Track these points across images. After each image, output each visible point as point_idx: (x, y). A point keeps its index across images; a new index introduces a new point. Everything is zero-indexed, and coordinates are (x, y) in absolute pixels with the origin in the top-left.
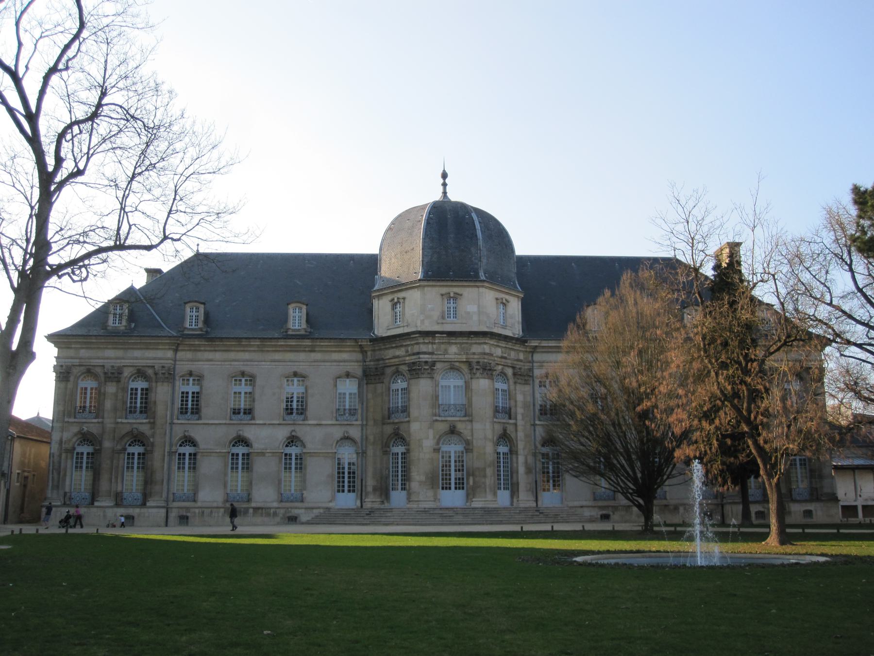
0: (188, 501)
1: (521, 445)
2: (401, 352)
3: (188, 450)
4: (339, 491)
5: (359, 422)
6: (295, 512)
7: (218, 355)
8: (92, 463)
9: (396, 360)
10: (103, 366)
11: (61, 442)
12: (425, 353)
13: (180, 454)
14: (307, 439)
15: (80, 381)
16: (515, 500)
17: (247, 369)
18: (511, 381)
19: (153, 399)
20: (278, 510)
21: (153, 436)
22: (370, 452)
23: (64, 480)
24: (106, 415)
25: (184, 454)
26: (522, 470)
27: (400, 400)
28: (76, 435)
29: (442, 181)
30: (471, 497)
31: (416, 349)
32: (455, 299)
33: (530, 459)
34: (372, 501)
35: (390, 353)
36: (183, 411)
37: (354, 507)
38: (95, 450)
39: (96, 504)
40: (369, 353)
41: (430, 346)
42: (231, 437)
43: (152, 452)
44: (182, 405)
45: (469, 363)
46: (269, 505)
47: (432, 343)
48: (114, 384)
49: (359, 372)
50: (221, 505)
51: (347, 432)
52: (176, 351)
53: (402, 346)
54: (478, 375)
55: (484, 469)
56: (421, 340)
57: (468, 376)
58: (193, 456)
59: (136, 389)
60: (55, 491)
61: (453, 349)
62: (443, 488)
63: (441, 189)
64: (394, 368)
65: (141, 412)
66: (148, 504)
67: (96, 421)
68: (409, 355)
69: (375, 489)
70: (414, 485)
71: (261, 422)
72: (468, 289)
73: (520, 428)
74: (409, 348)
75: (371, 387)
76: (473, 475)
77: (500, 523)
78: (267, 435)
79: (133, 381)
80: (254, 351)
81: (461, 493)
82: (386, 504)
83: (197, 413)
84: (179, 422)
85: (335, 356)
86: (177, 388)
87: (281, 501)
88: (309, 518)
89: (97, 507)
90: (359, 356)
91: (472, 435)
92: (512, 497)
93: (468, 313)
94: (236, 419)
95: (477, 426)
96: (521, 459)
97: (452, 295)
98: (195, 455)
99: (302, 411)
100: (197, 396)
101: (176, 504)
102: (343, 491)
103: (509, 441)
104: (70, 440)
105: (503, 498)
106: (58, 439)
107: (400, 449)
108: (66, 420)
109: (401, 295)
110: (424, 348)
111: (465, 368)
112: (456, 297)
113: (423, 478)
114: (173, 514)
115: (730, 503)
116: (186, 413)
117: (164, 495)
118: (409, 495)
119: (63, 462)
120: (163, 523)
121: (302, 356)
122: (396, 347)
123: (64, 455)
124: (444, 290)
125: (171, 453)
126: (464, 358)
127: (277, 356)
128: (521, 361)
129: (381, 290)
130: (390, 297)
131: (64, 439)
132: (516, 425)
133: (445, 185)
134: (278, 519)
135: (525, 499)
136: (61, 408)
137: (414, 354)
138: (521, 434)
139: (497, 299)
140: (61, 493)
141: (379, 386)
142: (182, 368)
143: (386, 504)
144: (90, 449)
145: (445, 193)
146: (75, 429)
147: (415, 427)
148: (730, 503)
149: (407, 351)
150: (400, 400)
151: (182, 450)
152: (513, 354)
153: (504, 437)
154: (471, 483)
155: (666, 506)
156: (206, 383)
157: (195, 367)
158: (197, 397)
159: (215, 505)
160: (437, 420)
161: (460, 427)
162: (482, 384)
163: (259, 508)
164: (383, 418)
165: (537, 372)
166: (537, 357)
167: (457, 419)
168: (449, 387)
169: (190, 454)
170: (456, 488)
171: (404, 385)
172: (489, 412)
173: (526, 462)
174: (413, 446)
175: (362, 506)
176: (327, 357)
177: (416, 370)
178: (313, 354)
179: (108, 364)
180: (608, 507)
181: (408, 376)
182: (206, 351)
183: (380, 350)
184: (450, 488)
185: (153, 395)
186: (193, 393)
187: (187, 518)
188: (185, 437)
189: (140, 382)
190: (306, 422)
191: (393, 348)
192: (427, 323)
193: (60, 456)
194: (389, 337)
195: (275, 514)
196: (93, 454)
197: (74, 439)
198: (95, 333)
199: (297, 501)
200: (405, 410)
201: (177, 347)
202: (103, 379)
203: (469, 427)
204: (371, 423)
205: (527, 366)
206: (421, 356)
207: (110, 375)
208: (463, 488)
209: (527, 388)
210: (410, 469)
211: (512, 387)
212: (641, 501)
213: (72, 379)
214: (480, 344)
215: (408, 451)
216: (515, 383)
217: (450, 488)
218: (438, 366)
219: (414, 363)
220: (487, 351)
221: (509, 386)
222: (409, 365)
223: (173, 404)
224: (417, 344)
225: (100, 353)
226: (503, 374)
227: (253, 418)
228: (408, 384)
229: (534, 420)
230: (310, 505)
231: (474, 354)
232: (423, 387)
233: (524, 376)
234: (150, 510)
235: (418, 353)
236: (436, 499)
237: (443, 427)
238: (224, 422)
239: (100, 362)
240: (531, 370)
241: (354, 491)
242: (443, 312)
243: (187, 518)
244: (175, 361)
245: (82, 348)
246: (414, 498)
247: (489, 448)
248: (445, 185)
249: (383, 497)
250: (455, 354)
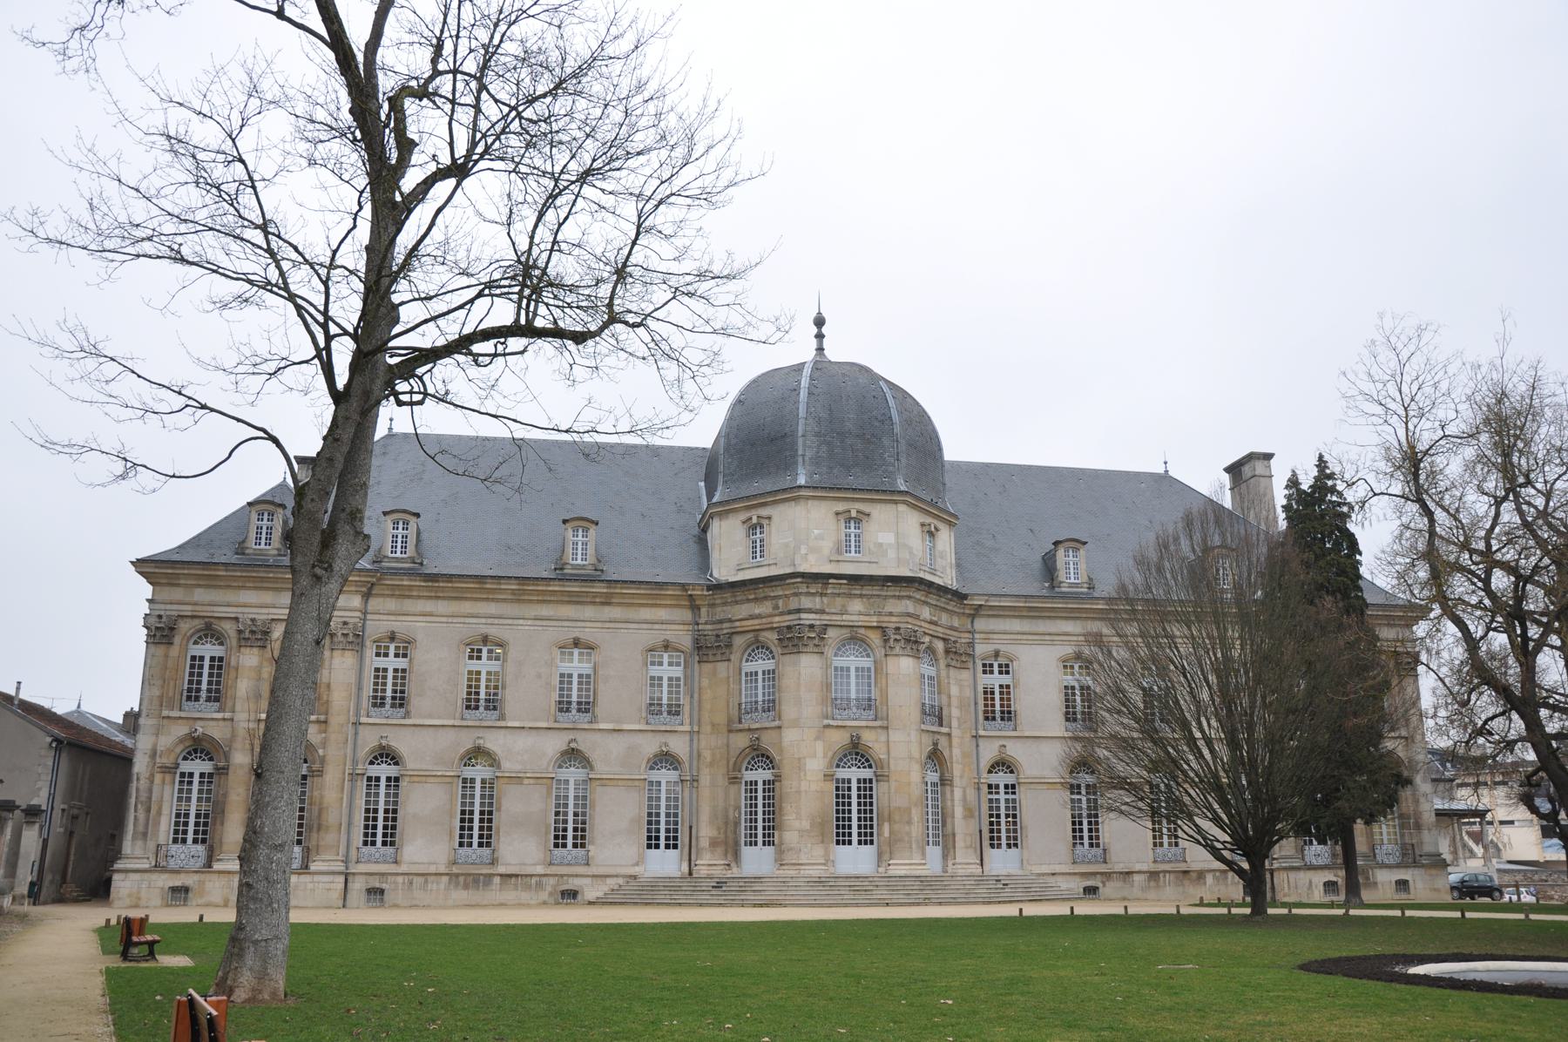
0: (385, 862)
1: (957, 770)
2: (764, 608)
3: (384, 770)
4: (649, 846)
5: (687, 728)
6: (573, 884)
7: (442, 607)
8: (209, 791)
9: (756, 622)
10: (236, 619)
11: (154, 754)
12: (810, 611)
13: (369, 779)
14: (595, 757)
15: (191, 645)
16: (950, 863)
17: (493, 631)
18: (942, 663)
19: (325, 680)
20: (544, 880)
21: (324, 744)
22: (705, 780)
23: (157, 823)
24: (238, 707)
25: (378, 779)
26: (959, 811)
27: (760, 691)
28: (181, 741)
29: (815, 330)
30: (886, 857)
31: (794, 604)
32: (858, 521)
33: (971, 794)
34: (709, 864)
35: (743, 610)
36: (378, 702)
37: (678, 874)
38: (217, 768)
39: (217, 866)
40: (704, 610)
41: (818, 599)
42: (462, 750)
43: (320, 773)
44: (375, 691)
45: (882, 629)
46: (529, 870)
47: (822, 595)
48: (255, 650)
49: (685, 639)
50: (442, 870)
51: (666, 745)
52: (367, 596)
53: (766, 598)
54: (897, 650)
55: (909, 810)
56: (803, 589)
57: (879, 653)
58: (393, 781)
59: (202, 658)
60: (140, 843)
61: (856, 606)
62: (838, 843)
63: (814, 343)
64: (750, 635)
65: (208, 699)
66: (313, 867)
67: (220, 715)
68: (782, 614)
69: (714, 844)
70: (790, 837)
71: (517, 724)
72: (879, 506)
73: (955, 741)
74: (780, 603)
75: (707, 667)
76: (889, 820)
77: (954, 902)
78: (525, 747)
79: (196, 643)
80: (504, 600)
81: (868, 851)
82: (735, 870)
83: (401, 705)
84: (371, 721)
85: (646, 613)
86: (367, 661)
87: (551, 864)
88: (600, 894)
89: (220, 872)
90: (687, 615)
91: (889, 753)
92: (945, 857)
93: (881, 545)
94: (565, 720)
95: (895, 736)
96: (958, 793)
97: (854, 514)
98: (397, 779)
99: (585, 707)
100: (400, 674)
101: (362, 868)
102: (657, 846)
103: (941, 765)
104: (170, 751)
105: (931, 862)
106: (149, 746)
107: (761, 775)
108: (165, 713)
109: (764, 512)
110: (806, 602)
111: (875, 638)
112: (859, 520)
113: (806, 825)
114: (358, 885)
115: (1285, 869)
116: (382, 705)
117: (342, 850)
118: (780, 853)
119: (156, 789)
120: (340, 903)
121: (588, 612)
122: (756, 600)
123: (158, 778)
124: (841, 507)
125: (354, 776)
126: (874, 621)
127: (545, 611)
128: (955, 629)
129: (728, 502)
130: (743, 516)
131: (159, 749)
132: (949, 735)
133: (820, 336)
134: (544, 896)
135: (965, 860)
136: (156, 692)
137: (790, 612)
138: (956, 752)
139: (923, 525)
140: (151, 845)
141: (722, 666)
142: (377, 626)
143: (735, 870)
144: (207, 767)
145: (820, 349)
146: (182, 730)
147: (790, 736)
148: (1285, 869)
149: (776, 607)
150: (760, 691)
151: (374, 771)
152: (944, 619)
153: (935, 757)
154: (886, 834)
155: (1185, 872)
156: (418, 654)
157: (400, 626)
158: (403, 678)
159: (432, 869)
160: (828, 726)
161: (868, 738)
162: (904, 666)
163: (510, 876)
164: (730, 721)
165: (981, 649)
166: (980, 624)
167: (864, 723)
168: (848, 669)
169: (389, 779)
170: (860, 843)
171: (769, 664)
172: (916, 714)
173: (964, 799)
174: (786, 770)
175: (690, 874)
176: (632, 614)
177: (793, 640)
178: (607, 609)
179: (247, 614)
180: (1094, 874)
181: (777, 650)
182: (419, 597)
183: (725, 604)
184: (850, 843)
185: (325, 672)
186: (580, 676)
187: (382, 891)
188: (382, 747)
189: (208, 646)
190: (595, 726)
191: (748, 601)
192: (812, 558)
193: (152, 776)
194: (743, 583)
195: (539, 886)
196: (211, 775)
197: (178, 750)
198: (223, 560)
199: (577, 864)
200: (771, 706)
201: (370, 589)
202: (234, 642)
203: (883, 738)
204: (707, 728)
205: (965, 638)
206: (803, 616)
207: (247, 635)
208: (872, 842)
209: (965, 675)
210: (781, 809)
211: (943, 673)
212: (1246, 866)
213: (177, 640)
214: (900, 598)
215: (778, 778)
216: (948, 666)
217: (850, 843)
218: (831, 633)
219: (789, 627)
220: (911, 610)
221: (938, 671)
222: (779, 630)
223: (360, 689)
224: (796, 594)
225: (230, 596)
226: (931, 650)
227: (502, 717)
228: (777, 664)
229: (357, 714)
230: (601, 871)
231: (891, 614)
232: (805, 669)
233: (958, 655)
234: (317, 878)
235: (799, 611)
236: (828, 861)
237: (840, 739)
238: (451, 722)
239: (231, 611)
240: (971, 644)
241: (675, 847)
242: (839, 542)
243: (382, 891)
244: (365, 613)
245: (199, 586)
246: (789, 858)
247: (915, 776)
248: (820, 336)
249: (730, 856)
250: (860, 614)
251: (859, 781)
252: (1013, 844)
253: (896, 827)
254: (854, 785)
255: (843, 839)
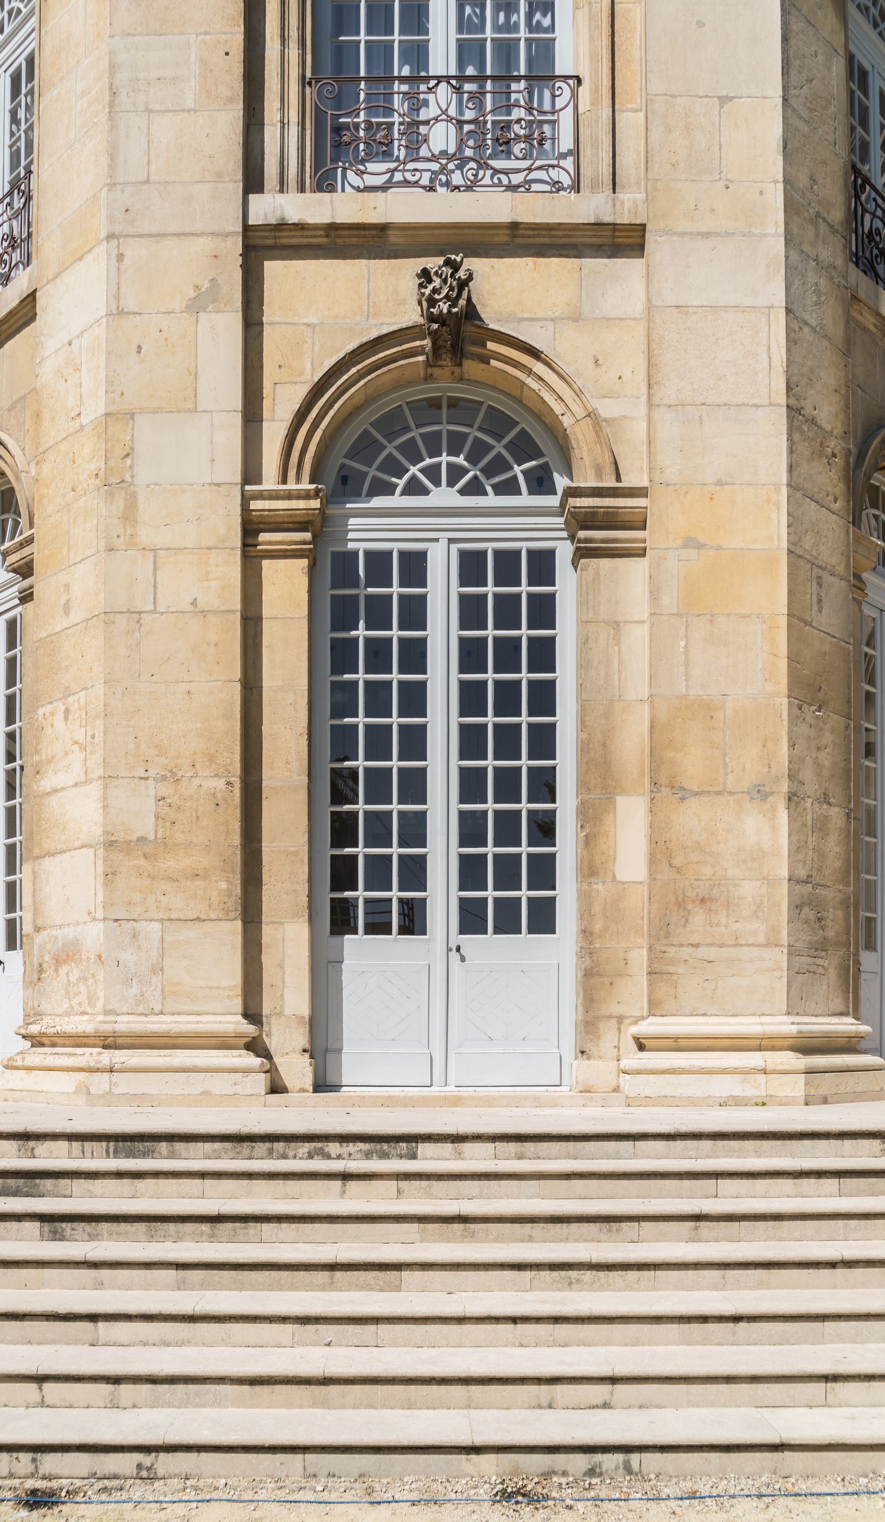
30: (632, 993)
170: (471, 919)
184: (413, 920)
208: (543, 919)
217: (413, 920)
251: (471, 566)
252: (512, 891)
253: (690, 819)
254: (442, 590)
255: (360, 891)
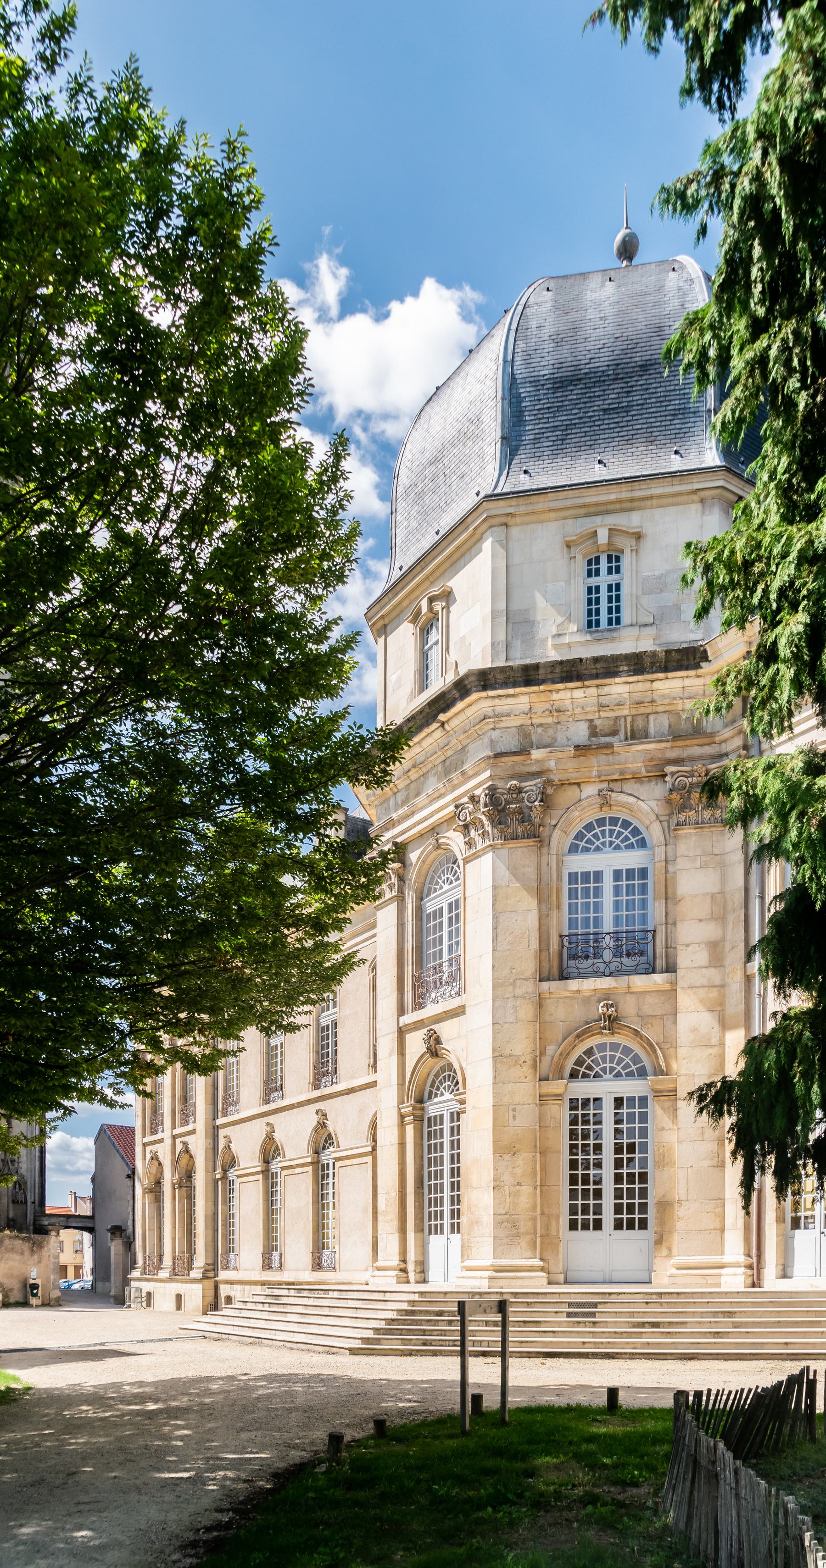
170: (618, 1226)
217: (598, 1225)
255: (584, 1219)
